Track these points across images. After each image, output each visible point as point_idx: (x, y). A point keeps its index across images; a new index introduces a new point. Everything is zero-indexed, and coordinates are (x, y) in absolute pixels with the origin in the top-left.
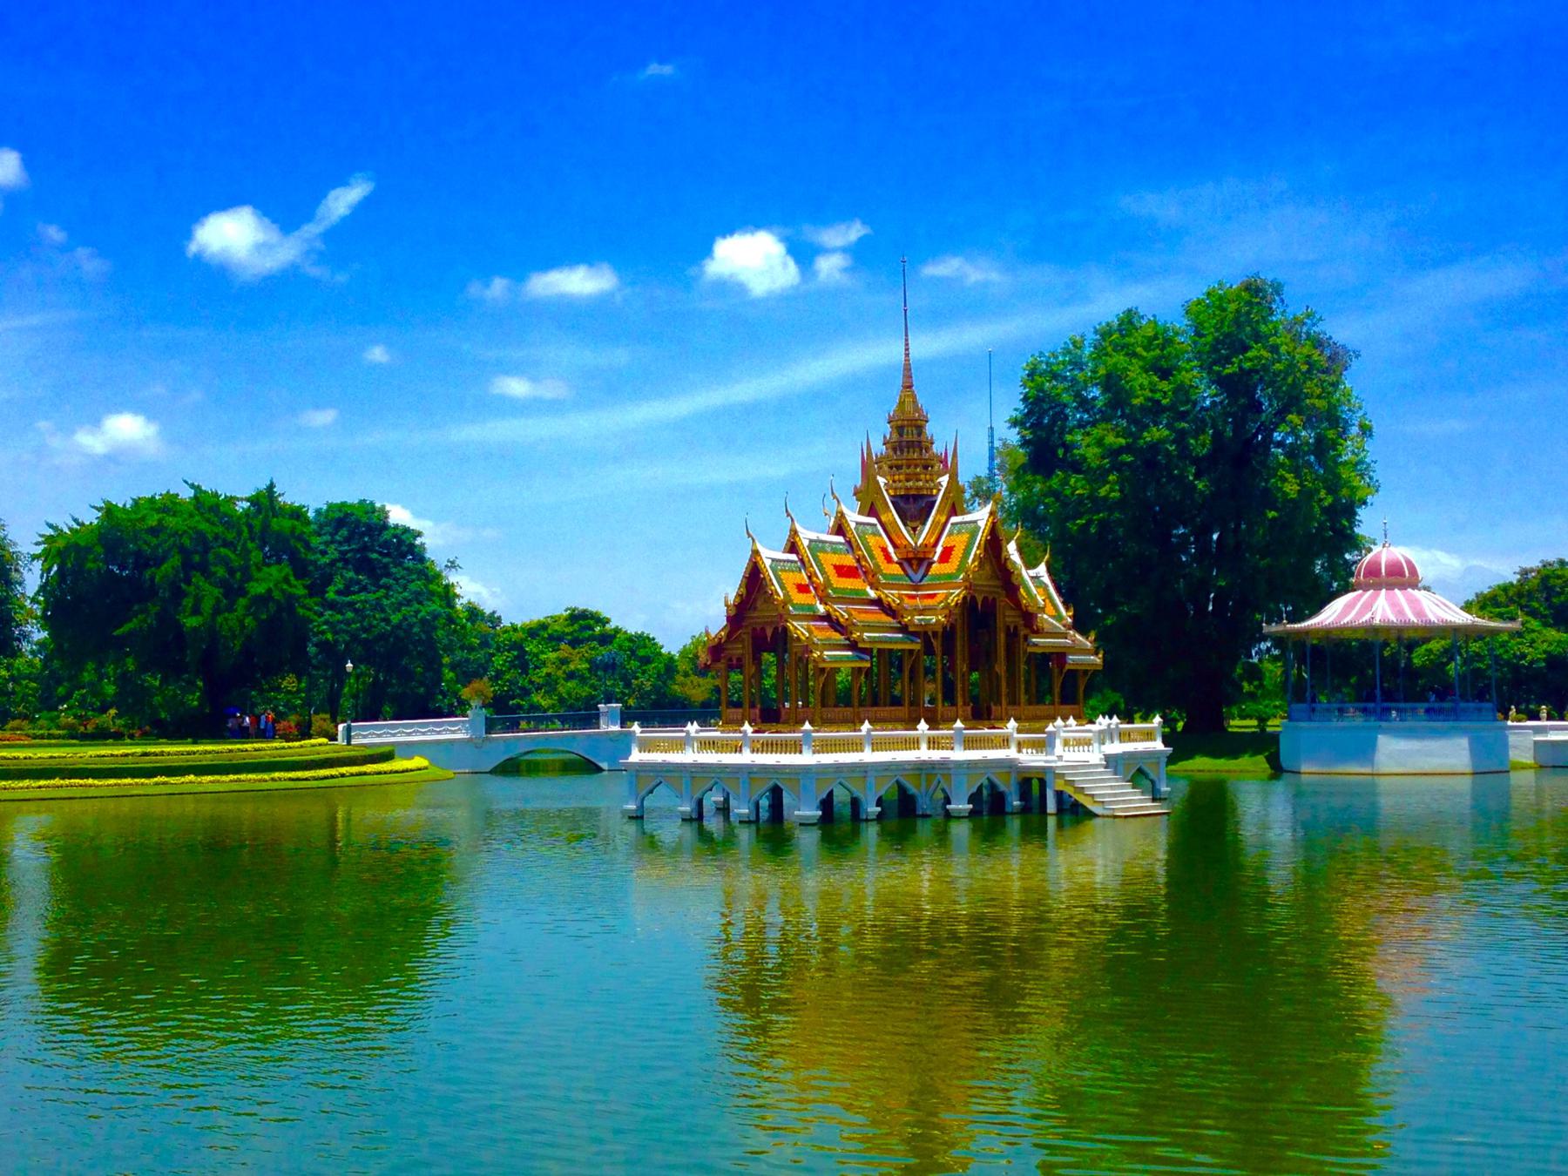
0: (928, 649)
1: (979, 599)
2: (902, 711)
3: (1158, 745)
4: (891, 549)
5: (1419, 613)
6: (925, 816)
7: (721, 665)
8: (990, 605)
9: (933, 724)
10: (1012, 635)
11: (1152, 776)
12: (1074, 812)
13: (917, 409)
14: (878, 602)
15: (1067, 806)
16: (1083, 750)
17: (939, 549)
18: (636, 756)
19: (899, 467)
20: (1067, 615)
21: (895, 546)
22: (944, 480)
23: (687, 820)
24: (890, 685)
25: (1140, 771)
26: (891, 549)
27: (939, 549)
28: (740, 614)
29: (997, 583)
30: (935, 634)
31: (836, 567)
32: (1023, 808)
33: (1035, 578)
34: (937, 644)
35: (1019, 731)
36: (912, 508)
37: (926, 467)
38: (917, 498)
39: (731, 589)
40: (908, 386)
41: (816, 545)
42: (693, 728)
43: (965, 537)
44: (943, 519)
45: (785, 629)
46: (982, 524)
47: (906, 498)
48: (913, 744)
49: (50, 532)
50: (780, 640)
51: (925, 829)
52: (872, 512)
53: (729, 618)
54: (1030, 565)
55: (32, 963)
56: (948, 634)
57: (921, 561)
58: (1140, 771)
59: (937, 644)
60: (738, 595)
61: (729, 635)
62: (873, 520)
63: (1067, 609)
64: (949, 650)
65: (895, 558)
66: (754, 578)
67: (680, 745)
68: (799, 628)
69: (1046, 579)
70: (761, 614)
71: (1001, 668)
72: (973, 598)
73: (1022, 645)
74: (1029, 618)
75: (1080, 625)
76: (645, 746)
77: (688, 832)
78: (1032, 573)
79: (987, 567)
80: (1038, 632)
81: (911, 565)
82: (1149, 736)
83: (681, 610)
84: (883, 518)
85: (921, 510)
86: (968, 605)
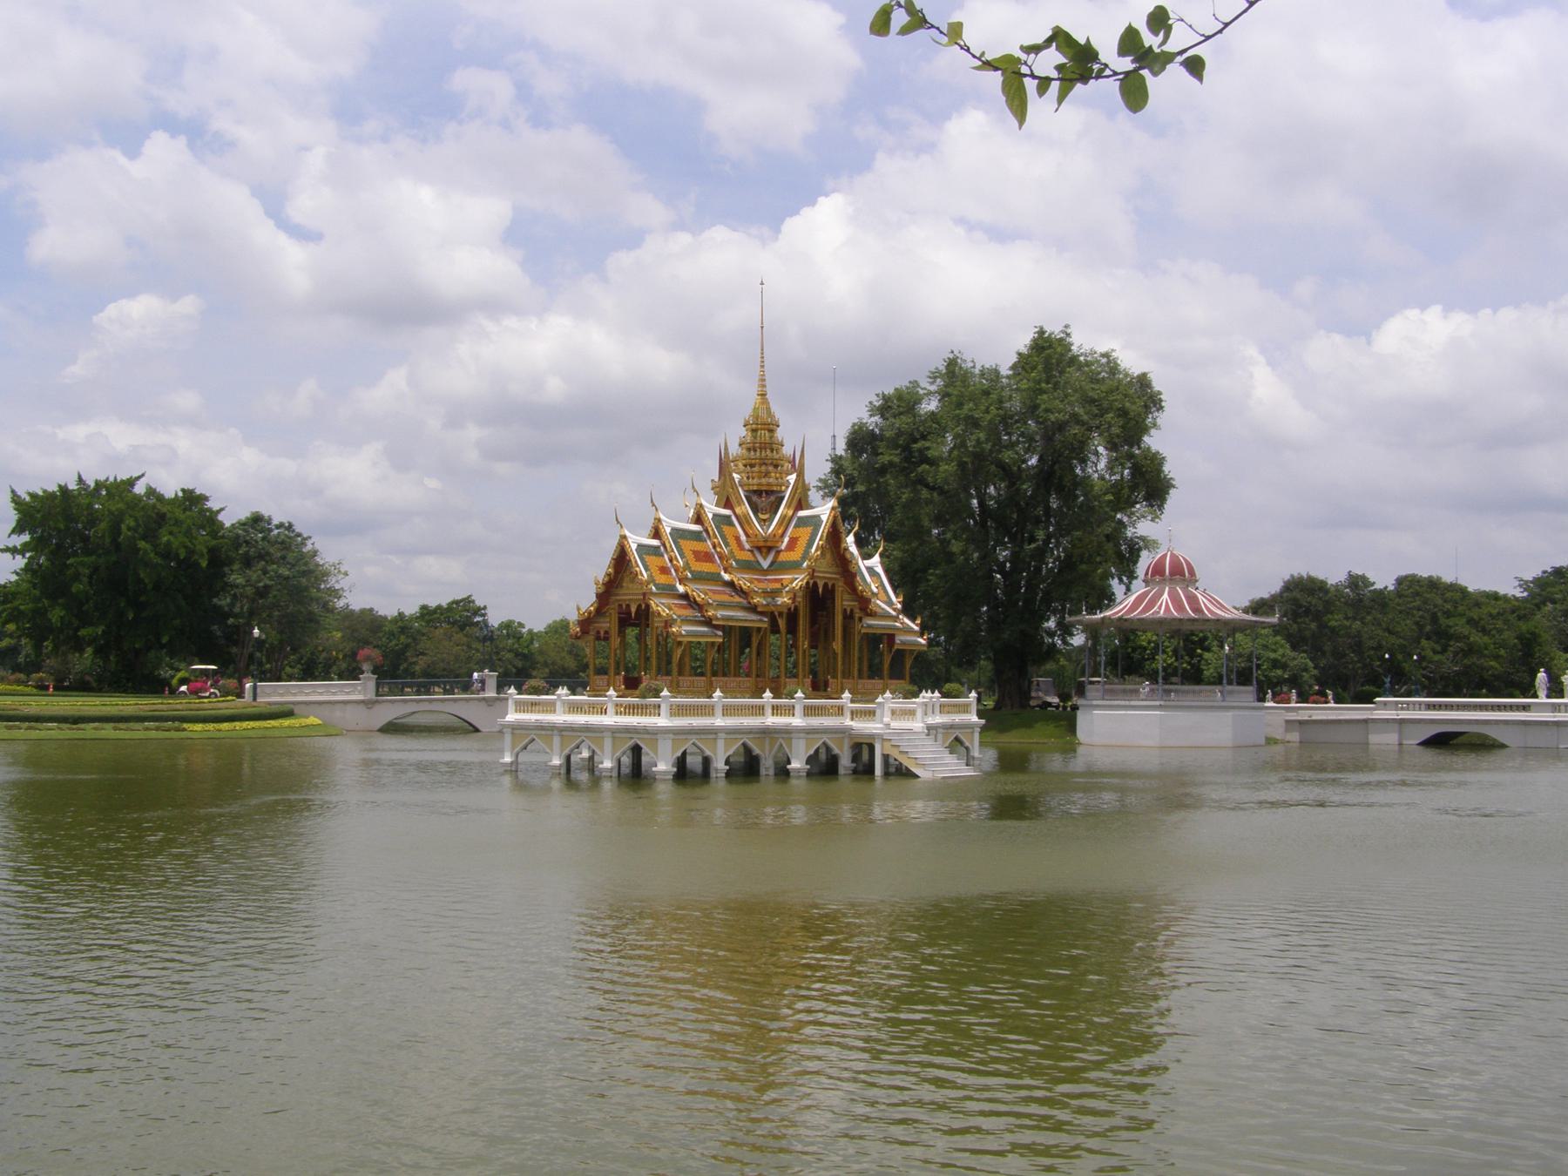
0: (775, 629)
3: (974, 718)
4: (743, 538)
5: (1197, 610)
8: (830, 592)
9: (777, 694)
14: (731, 584)
17: (786, 540)
18: (512, 717)
21: (747, 535)
22: (792, 478)
27: (786, 540)
30: (781, 614)
33: (870, 570)
37: (776, 466)
41: (678, 534)
43: (810, 529)
45: (648, 606)
46: (824, 518)
47: (759, 493)
48: (708, 711)
52: (728, 504)
56: (792, 616)
57: (770, 549)
62: (727, 512)
65: (747, 546)
66: (621, 560)
68: (661, 607)
69: (879, 570)
72: (815, 584)
79: (828, 556)
80: (873, 615)
82: (965, 709)
84: (738, 510)
86: (811, 590)
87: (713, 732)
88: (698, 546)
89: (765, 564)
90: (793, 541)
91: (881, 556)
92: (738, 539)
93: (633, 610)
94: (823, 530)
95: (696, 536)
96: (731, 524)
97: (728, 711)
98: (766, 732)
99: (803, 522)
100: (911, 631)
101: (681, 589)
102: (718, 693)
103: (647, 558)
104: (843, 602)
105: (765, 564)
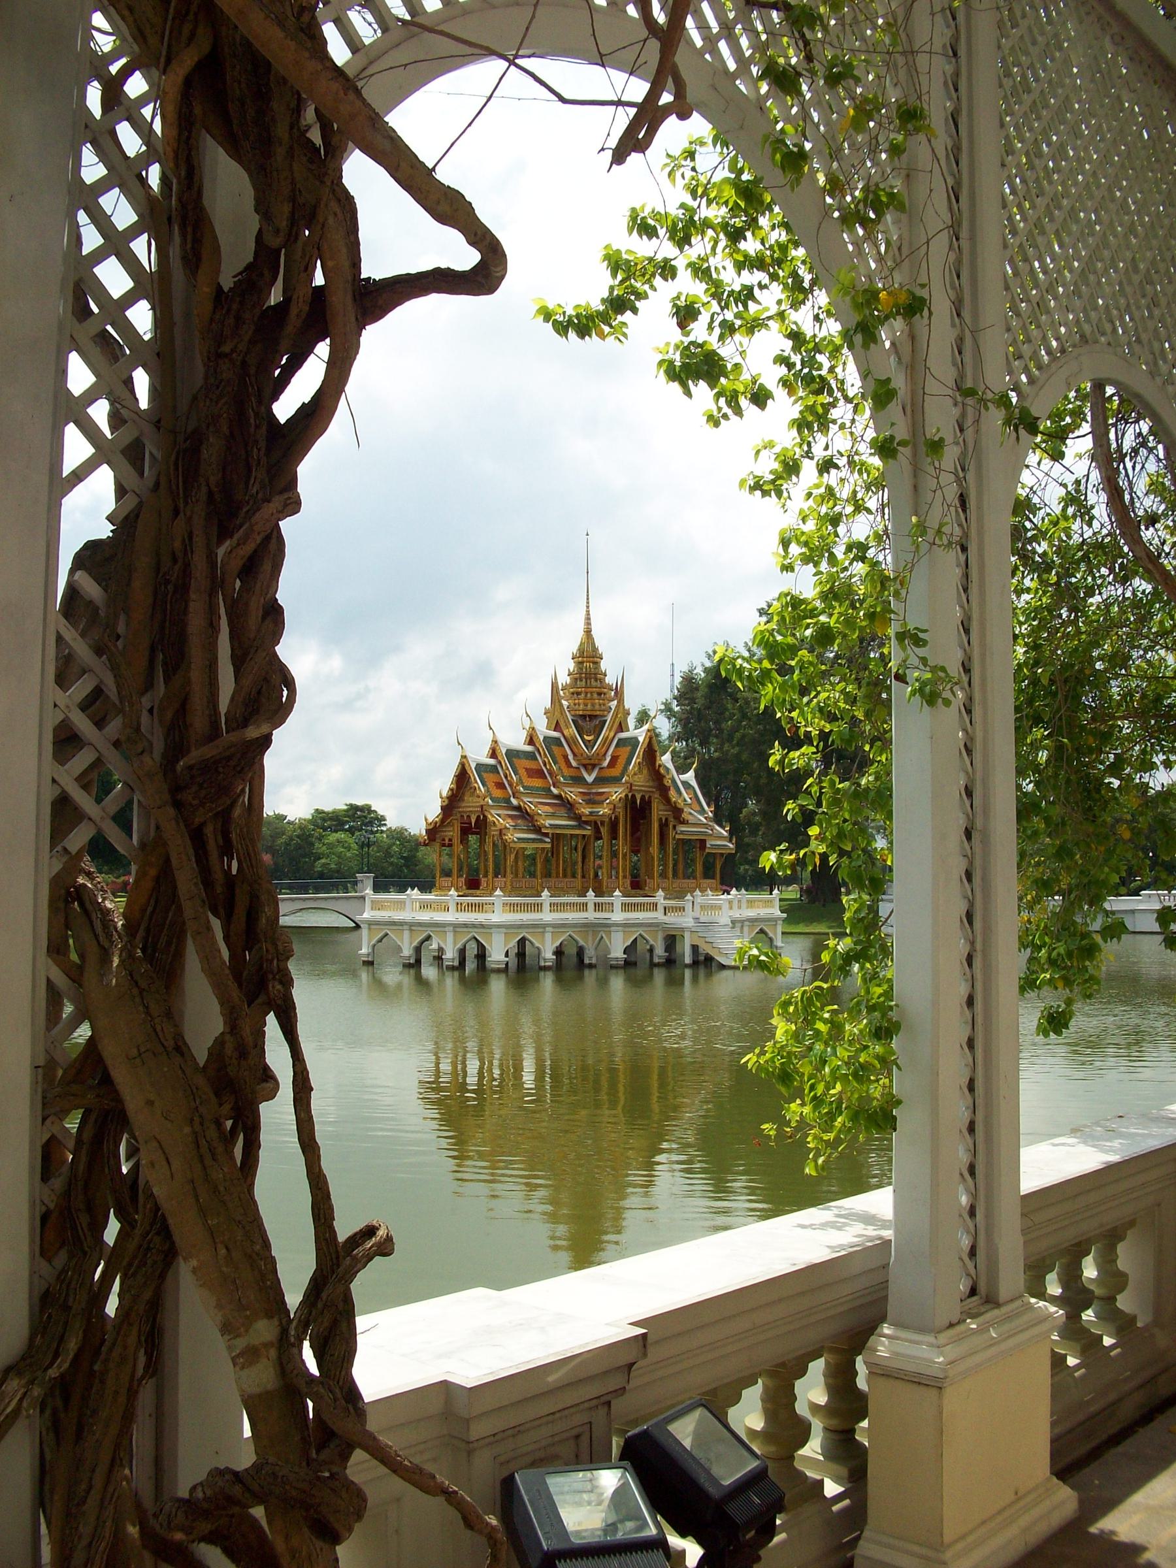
1: (638, 797)
2: (578, 882)
3: (777, 912)
4: (571, 757)
6: (591, 966)
7: (437, 846)
8: (646, 804)
9: (599, 893)
10: (663, 826)
11: (771, 935)
12: (705, 963)
13: (595, 649)
15: (702, 958)
16: (724, 918)
19: (578, 694)
20: (709, 811)
21: (574, 755)
22: (614, 704)
23: (408, 966)
24: (562, 863)
25: (762, 931)
26: (571, 757)
27: (608, 759)
28: (451, 804)
29: (651, 784)
31: (526, 769)
32: (673, 963)
33: (686, 785)
34: (604, 831)
35: (665, 898)
36: (587, 725)
38: (592, 717)
39: (444, 783)
40: (588, 632)
42: (414, 893)
44: (612, 734)
46: (641, 739)
47: (583, 717)
48: (538, 907)
49: (1022, 432)
50: (481, 826)
51: (590, 977)
53: (442, 807)
54: (682, 770)
55: (271, 505)
56: (614, 825)
57: (594, 766)
58: (762, 931)
59: (604, 831)
60: (451, 790)
61: (443, 821)
63: (709, 806)
64: (614, 835)
65: (574, 764)
66: (462, 777)
67: (401, 905)
69: (694, 783)
70: (470, 805)
71: (654, 849)
72: (633, 796)
73: (671, 833)
74: (677, 812)
75: (718, 819)
76: (376, 905)
77: (407, 979)
78: (684, 777)
79: (645, 772)
80: (684, 822)
81: (586, 769)
82: (768, 903)
83: (410, 806)
85: (596, 726)
87: (540, 927)
88: (530, 764)
89: (590, 779)
90: (614, 759)
91: (696, 771)
92: (566, 757)
93: (473, 821)
94: (639, 751)
95: (531, 756)
96: (561, 745)
97: (554, 907)
98: (588, 927)
99: (622, 743)
100: (721, 837)
101: (514, 802)
102: (546, 893)
103: (485, 775)
104: (658, 811)
105: (590, 779)
